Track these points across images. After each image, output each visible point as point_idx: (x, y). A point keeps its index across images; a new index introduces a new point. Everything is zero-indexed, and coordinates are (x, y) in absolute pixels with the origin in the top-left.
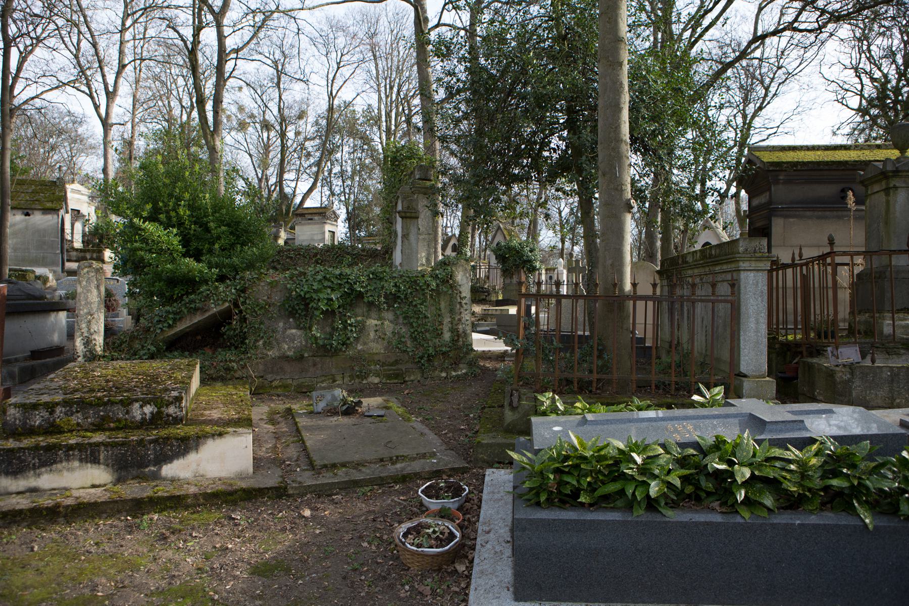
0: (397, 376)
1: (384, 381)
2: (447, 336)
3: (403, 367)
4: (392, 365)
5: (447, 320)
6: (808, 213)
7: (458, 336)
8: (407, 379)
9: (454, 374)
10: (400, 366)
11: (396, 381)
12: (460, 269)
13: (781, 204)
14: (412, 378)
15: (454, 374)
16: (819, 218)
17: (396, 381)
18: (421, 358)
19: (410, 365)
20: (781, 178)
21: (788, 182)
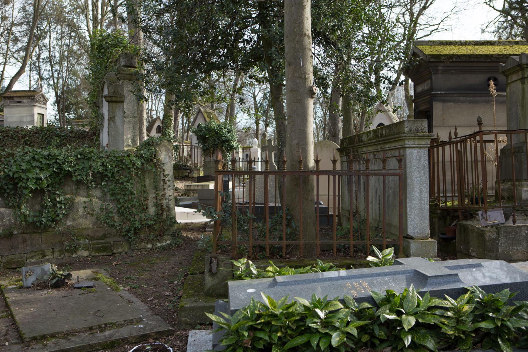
0: (105, 249)
1: (93, 254)
2: (152, 210)
3: (111, 241)
4: (100, 238)
5: (151, 196)
6: (462, 98)
7: (163, 210)
8: (115, 251)
9: (159, 245)
10: (108, 240)
11: (105, 254)
12: (163, 149)
13: (440, 90)
14: (120, 250)
15: (159, 245)
16: (471, 102)
17: (105, 254)
18: (128, 231)
19: (117, 238)
20: (440, 68)
21: (445, 72)
